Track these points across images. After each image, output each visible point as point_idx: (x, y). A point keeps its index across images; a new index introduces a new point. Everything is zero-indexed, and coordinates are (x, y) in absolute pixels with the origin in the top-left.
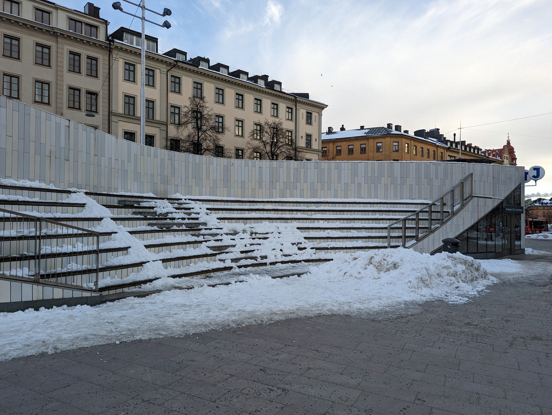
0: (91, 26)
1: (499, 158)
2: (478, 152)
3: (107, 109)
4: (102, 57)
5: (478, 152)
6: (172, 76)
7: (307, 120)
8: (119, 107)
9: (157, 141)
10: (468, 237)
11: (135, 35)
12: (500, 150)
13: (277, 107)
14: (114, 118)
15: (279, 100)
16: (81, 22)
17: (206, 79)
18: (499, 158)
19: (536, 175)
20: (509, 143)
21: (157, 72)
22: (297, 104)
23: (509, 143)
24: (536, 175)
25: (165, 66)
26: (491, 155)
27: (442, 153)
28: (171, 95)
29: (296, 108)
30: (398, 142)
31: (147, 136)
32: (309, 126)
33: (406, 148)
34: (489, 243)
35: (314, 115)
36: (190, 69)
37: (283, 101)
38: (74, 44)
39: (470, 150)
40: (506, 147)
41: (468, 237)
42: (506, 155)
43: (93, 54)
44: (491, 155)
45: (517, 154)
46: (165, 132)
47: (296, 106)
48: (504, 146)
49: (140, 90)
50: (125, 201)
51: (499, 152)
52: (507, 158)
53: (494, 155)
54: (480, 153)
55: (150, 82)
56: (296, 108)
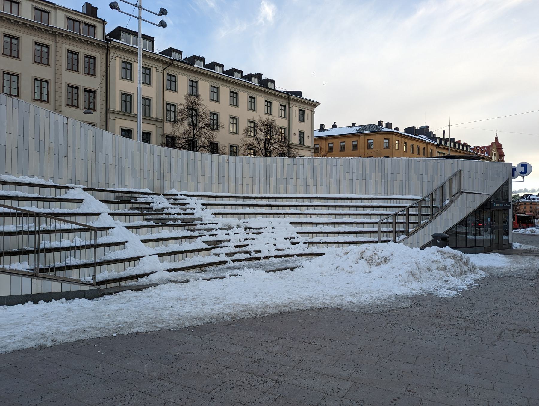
0: (89, 25)
1: (487, 155)
2: (467, 149)
3: (104, 107)
4: (99, 55)
5: (467, 149)
6: (168, 74)
7: (300, 117)
8: (116, 104)
9: (153, 138)
10: (457, 232)
11: (132, 34)
12: (488, 147)
13: (271, 105)
14: (111, 116)
15: (273, 97)
16: (79, 22)
17: (202, 77)
18: (487, 155)
19: (523, 171)
20: (497, 139)
21: (154, 71)
22: (290, 102)
23: (497, 139)
24: (523, 171)
25: (161, 65)
26: (480, 151)
27: (431, 150)
28: (167, 93)
29: (289, 106)
30: (389, 139)
31: (144, 133)
32: (301, 124)
33: (397, 145)
34: (478, 237)
35: (307, 112)
36: (185, 68)
37: (276, 98)
38: (73, 43)
39: (459, 147)
40: (494, 144)
41: (457, 232)
42: (494, 152)
43: (91, 53)
44: (480, 151)
45: (505, 151)
46: (161, 129)
47: (289, 103)
48: (492, 143)
49: (137, 89)
50: (122, 196)
51: (488, 149)
52: (495, 155)
53: (482, 152)
54: (468, 150)
55: (147, 80)
56: (289, 106)
